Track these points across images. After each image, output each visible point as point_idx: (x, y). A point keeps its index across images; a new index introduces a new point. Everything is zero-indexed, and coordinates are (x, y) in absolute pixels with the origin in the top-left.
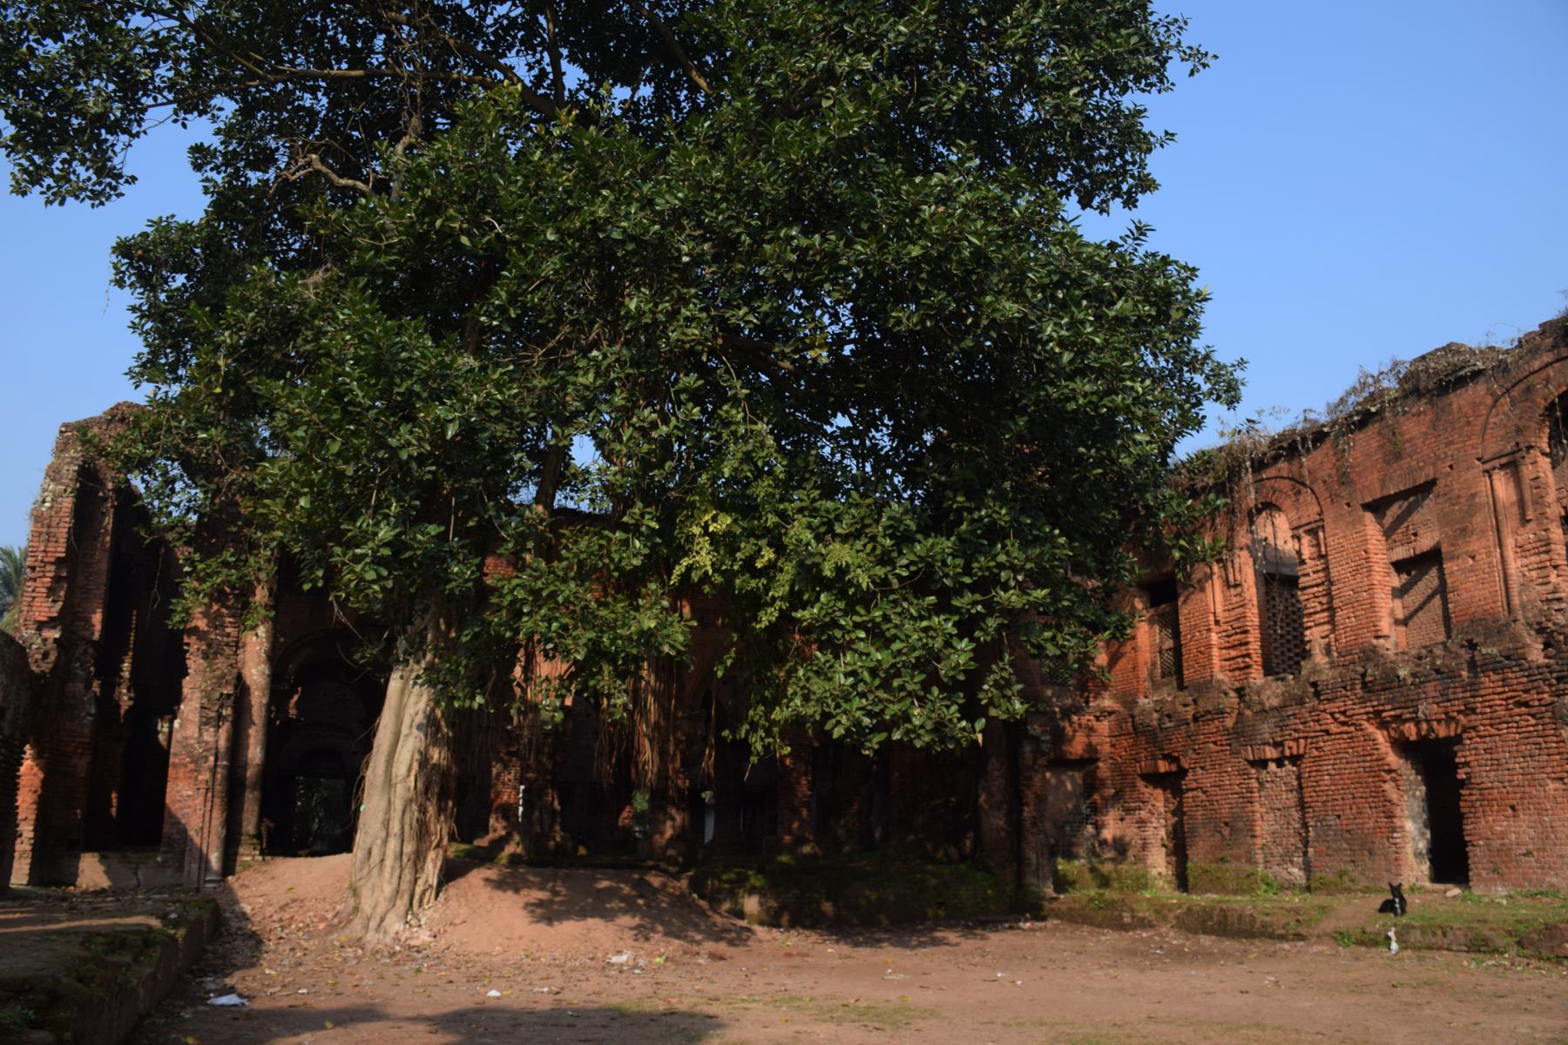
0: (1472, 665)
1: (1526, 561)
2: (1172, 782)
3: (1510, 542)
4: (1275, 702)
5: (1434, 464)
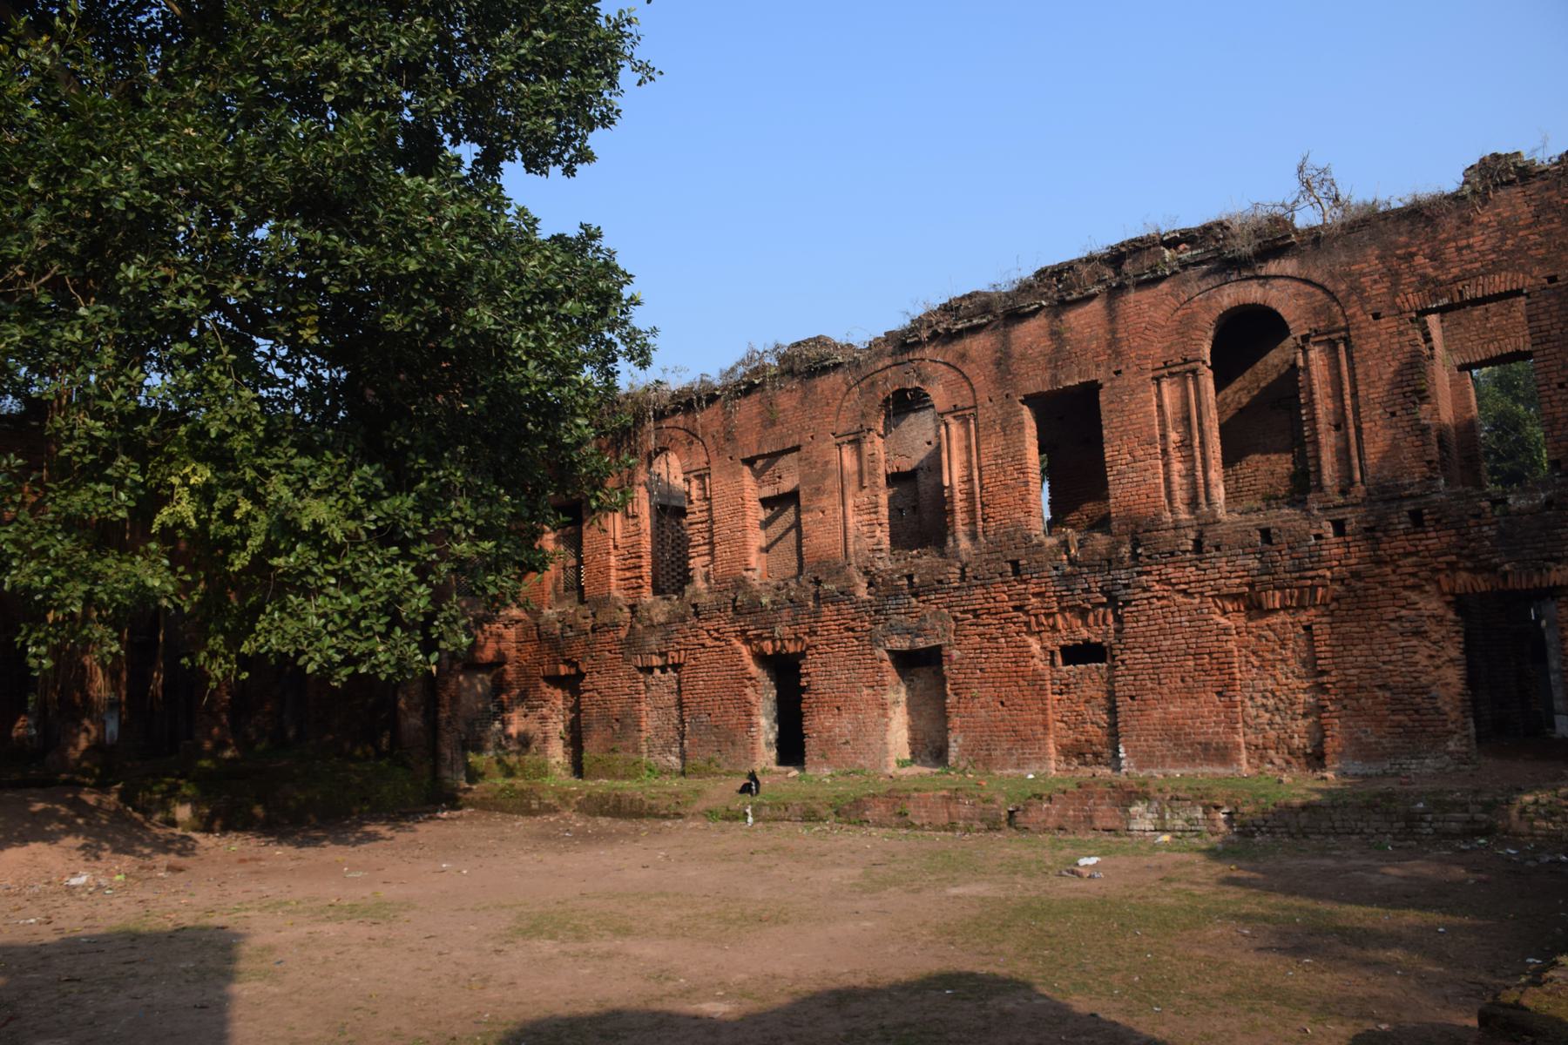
0: (817, 597)
1: (860, 518)
2: (571, 684)
3: (850, 502)
4: (662, 619)
5: (799, 433)
